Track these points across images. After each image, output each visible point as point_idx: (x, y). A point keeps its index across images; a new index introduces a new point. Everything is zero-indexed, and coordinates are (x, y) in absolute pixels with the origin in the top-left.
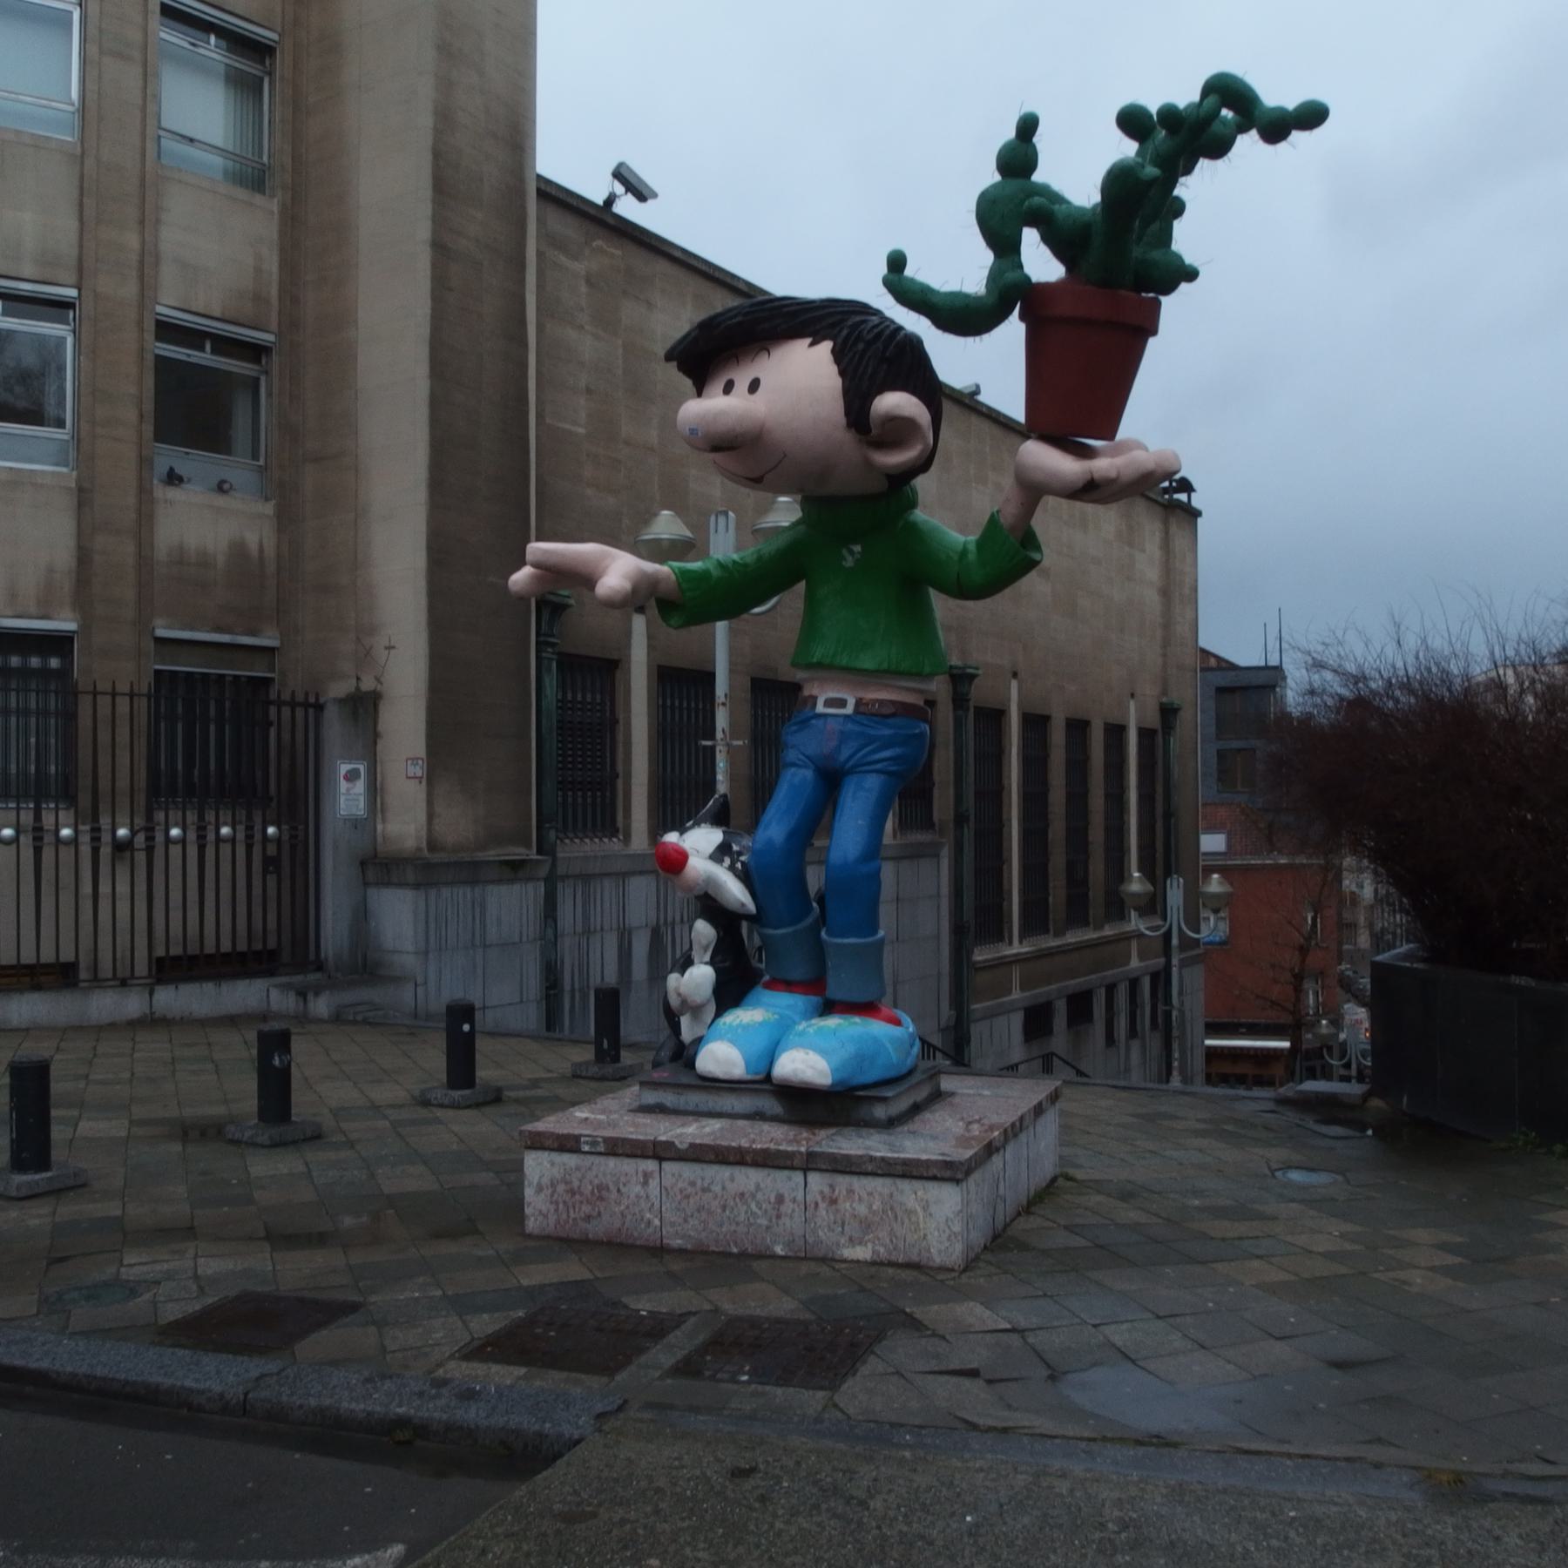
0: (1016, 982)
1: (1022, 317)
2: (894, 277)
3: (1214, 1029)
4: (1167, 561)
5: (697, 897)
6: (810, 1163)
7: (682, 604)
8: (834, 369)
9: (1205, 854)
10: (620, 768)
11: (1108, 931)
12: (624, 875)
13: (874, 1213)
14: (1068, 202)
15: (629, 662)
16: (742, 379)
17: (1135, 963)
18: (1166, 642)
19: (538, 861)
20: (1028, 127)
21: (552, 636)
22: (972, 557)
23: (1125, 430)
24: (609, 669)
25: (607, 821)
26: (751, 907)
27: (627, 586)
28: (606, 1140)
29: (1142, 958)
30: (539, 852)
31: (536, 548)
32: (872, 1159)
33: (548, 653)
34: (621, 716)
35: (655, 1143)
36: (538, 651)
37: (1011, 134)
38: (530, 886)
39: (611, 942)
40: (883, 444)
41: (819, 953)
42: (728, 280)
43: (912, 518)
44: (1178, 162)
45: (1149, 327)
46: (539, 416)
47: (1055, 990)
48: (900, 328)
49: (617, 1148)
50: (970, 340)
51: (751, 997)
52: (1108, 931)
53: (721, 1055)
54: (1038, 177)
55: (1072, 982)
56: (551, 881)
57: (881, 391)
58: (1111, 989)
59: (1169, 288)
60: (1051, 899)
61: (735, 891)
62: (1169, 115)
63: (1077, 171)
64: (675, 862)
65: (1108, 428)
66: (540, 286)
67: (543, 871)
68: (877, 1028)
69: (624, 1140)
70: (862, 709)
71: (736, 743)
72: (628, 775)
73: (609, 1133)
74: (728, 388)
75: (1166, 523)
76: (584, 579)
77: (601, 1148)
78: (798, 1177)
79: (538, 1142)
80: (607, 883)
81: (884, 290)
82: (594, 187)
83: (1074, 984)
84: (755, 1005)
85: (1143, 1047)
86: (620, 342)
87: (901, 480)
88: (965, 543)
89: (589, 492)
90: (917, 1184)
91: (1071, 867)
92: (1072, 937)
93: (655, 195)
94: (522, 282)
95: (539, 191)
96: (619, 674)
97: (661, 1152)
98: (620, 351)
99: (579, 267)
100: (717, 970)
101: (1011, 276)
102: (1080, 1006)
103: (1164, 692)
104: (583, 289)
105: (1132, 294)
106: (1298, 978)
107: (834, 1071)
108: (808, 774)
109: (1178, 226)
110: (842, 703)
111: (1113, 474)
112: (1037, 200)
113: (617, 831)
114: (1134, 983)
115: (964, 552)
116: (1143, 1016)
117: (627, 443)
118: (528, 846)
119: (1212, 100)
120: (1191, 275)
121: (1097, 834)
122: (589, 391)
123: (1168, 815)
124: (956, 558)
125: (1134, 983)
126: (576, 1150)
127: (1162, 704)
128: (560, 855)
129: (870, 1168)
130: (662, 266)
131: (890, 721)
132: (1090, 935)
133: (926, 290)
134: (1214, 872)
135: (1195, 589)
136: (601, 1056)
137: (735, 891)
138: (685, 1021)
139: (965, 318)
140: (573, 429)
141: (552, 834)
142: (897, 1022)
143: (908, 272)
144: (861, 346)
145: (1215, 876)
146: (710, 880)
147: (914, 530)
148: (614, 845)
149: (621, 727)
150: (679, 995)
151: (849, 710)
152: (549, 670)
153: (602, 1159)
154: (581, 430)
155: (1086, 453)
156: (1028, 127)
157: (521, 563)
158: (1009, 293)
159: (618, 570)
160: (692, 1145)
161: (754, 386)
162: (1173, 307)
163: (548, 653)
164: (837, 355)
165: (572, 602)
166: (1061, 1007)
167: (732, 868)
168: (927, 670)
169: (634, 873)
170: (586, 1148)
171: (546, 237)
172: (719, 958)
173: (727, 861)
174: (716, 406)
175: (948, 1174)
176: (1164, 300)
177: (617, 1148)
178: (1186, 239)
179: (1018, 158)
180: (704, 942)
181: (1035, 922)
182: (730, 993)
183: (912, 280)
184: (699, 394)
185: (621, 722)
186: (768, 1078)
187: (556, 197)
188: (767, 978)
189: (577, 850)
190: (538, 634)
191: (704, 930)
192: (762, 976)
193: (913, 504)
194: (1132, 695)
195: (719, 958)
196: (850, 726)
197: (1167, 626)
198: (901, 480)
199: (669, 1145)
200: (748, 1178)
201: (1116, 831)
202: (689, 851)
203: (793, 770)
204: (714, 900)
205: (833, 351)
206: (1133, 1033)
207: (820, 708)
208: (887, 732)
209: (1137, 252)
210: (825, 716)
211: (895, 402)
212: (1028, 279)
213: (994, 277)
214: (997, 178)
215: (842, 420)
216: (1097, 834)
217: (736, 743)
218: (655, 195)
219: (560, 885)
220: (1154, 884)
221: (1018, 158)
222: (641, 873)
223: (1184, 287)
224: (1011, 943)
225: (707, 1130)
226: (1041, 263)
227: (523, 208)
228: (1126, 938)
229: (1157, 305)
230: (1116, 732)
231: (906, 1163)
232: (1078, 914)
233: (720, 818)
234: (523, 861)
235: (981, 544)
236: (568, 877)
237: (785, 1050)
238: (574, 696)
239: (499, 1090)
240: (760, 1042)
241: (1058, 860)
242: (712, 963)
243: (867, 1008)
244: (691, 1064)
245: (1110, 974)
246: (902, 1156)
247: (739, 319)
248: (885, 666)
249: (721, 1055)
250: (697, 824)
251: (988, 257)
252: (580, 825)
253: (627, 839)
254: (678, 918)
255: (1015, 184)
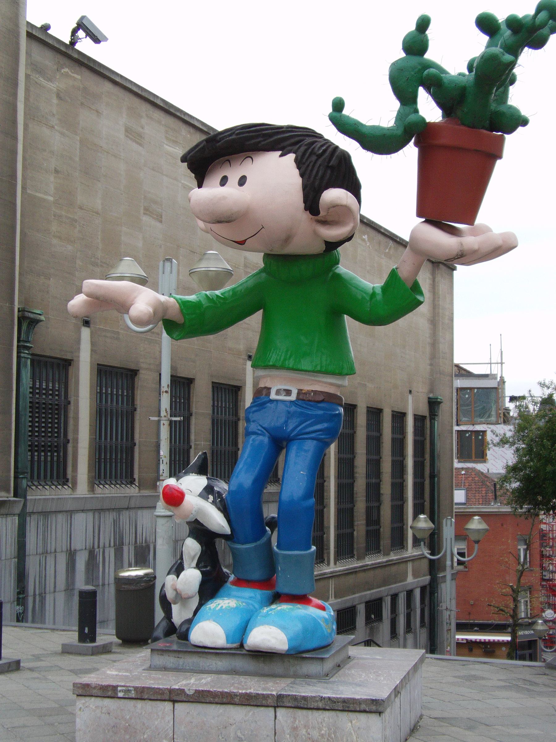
0: (332, 592)
1: (416, 144)
2: (336, 114)
3: (462, 627)
4: (434, 300)
5: (189, 523)
6: (279, 702)
7: (183, 323)
8: (297, 172)
9: (457, 504)
10: (70, 436)
11: (393, 557)
12: (71, 513)
13: (322, 736)
14: (448, 73)
15: (79, 361)
16: (234, 175)
17: (410, 579)
18: (433, 356)
19: (15, 502)
20: (423, 24)
21: (28, 341)
22: (379, 297)
23: (481, 218)
24: (64, 366)
25: (60, 475)
26: (227, 530)
27: (151, 310)
28: (136, 688)
29: (415, 576)
30: (15, 495)
31: (91, 284)
32: (322, 699)
33: (25, 354)
34: (72, 399)
35: (171, 691)
36: (18, 352)
37: (413, 27)
38: (9, 519)
39: (62, 560)
40: (324, 223)
41: (270, 562)
42: (152, 99)
43: (337, 271)
44: (515, 50)
45: (494, 154)
46: (24, 188)
47: (358, 598)
48: (337, 147)
49: (143, 694)
50: (384, 157)
51: (222, 591)
52: (393, 557)
53: (209, 630)
54: (428, 56)
55: (368, 592)
56: (23, 517)
57: (326, 188)
58: (394, 597)
59: (511, 130)
60: (355, 533)
61: (217, 520)
62: (514, 24)
63: (456, 52)
64: (175, 498)
65: (469, 216)
66: (27, 99)
67: (18, 509)
68: (311, 611)
69: (149, 688)
70: (301, 397)
71: (174, 419)
72: (76, 441)
73: (138, 684)
74: (224, 181)
75: (433, 274)
76: (123, 307)
77: (133, 694)
78: (272, 710)
79: (85, 691)
80: (60, 517)
81: (330, 123)
82: (62, 33)
83: (370, 594)
84: (229, 596)
85: (415, 638)
86: (79, 139)
87: (332, 246)
88: (373, 288)
89: (55, 241)
90: (352, 715)
91: (369, 510)
92: (370, 561)
93: (106, 39)
94: (15, 95)
95: (30, 35)
96: (71, 370)
97: (174, 697)
98: (78, 146)
99: (52, 86)
100: (202, 573)
101: (412, 117)
102: (374, 608)
103: (431, 391)
104: (55, 101)
105: (489, 132)
106: (515, 592)
107: (289, 640)
108: (266, 440)
109: (512, 89)
110: (288, 392)
111: (476, 247)
112: (432, 70)
113: (67, 480)
114: (410, 594)
115: (373, 295)
116: (415, 616)
117: (81, 208)
118: (8, 491)
119: (543, 15)
120: (524, 122)
121: (386, 489)
122: (57, 171)
123: (432, 476)
124: (368, 298)
125: (410, 594)
126: (114, 697)
127: (429, 398)
128: (28, 497)
129: (320, 705)
130: (108, 86)
131: (320, 405)
132: (381, 559)
133: (357, 124)
134: (475, 515)
135: (452, 320)
136: (83, 638)
137: (217, 520)
138: (175, 609)
139: (381, 143)
140: (46, 197)
141: (24, 482)
142: (323, 608)
143: (345, 112)
144: (314, 158)
145: (476, 518)
146: (200, 511)
147: (338, 277)
148: (65, 492)
149: (72, 407)
150: (176, 590)
151: (293, 397)
152: (26, 366)
153: (133, 702)
154: (51, 199)
155: (453, 231)
156: (423, 24)
157: (79, 291)
158: (411, 130)
159: (144, 301)
160: (197, 691)
161: (242, 181)
162: (512, 142)
163: (25, 354)
164: (299, 163)
165: (42, 318)
166: (361, 610)
167: (214, 503)
168: (345, 371)
169: (77, 511)
170: (120, 695)
171: (33, 66)
172: (202, 564)
173: (211, 498)
174: (213, 193)
175: (374, 708)
176: (508, 138)
177: (143, 694)
178: (517, 97)
179: (416, 44)
180: (192, 553)
181: (345, 549)
182: (210, 588)
183: (348, 117)
184: (200, 186)
185: (72, 402)
186: (242, 646)
187: (40, 37)
188: (232, 577)
189: (42, 495)
190: (19, 341)
191: (192, 547)
192: (228, 577)
193: (337, 262)
194: (410, 392)
195: (202, 564)
196: (293, 408)
197: (434, 344)
198: (332, 246)
199: (181, 691)
200: (237, 714)
201: (399, 488)
202: (185, 491)
203: (253, 437)
204: (202, 525)
205: (296, 160)
206: (409, 628)
207: (273, 396)
208: (320, 412)
209: (493, 106)
210: (277, 401)
211: (334, 195)
212: (423, 120)
213: (400, 117)
214: (403, 55)
215: (302, 205)
216: (386, 489)
217: (174, 419)
218: (106, 39)
219: (28, 519)
220: (433, 522)
221: (416, 44)
222: (83, 511)
223: (520, 129)
224: (328, 564)
225: (203, 681)
226: (429, 110)
227: (18, 44)
228: (405, 561)
229: (501, 140)
230: (399, 417)
231: (345, 701)
232: (374, 544)
233: (201, 470)
234: (5, 501)
235: (385, 289)
236: (33, 513)
237: (255, 627)
238: (41, 385)
239: (18, 662)
240: (235, 621)
241: (361, 506)
242: (198, 566)
243: (301, 599)
244: (185, 636)
245: (394, 587)
246: (343, 696)
247: (234, 137)
248: (318, 368)
249: (209, 630)
250: (186, 473)
251: (396, 104)
252: (36, 477)
253: (75, 484)
254: (107, 545)
255: (415, 60)
